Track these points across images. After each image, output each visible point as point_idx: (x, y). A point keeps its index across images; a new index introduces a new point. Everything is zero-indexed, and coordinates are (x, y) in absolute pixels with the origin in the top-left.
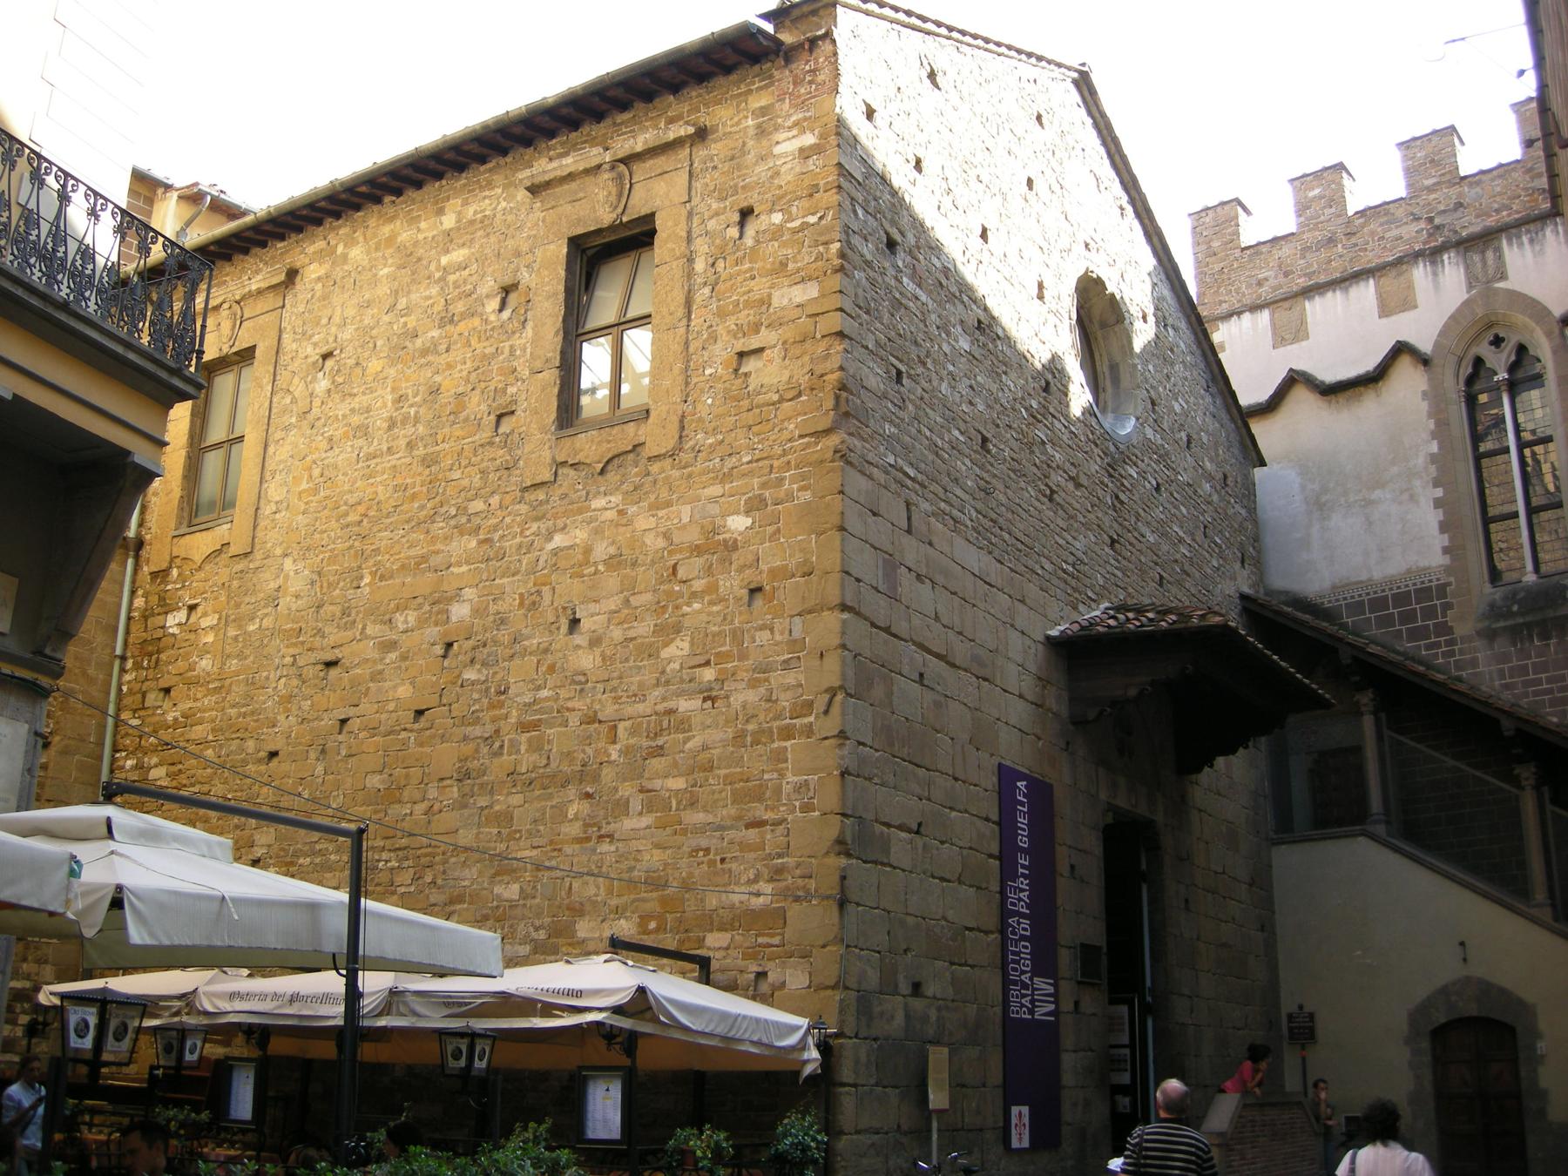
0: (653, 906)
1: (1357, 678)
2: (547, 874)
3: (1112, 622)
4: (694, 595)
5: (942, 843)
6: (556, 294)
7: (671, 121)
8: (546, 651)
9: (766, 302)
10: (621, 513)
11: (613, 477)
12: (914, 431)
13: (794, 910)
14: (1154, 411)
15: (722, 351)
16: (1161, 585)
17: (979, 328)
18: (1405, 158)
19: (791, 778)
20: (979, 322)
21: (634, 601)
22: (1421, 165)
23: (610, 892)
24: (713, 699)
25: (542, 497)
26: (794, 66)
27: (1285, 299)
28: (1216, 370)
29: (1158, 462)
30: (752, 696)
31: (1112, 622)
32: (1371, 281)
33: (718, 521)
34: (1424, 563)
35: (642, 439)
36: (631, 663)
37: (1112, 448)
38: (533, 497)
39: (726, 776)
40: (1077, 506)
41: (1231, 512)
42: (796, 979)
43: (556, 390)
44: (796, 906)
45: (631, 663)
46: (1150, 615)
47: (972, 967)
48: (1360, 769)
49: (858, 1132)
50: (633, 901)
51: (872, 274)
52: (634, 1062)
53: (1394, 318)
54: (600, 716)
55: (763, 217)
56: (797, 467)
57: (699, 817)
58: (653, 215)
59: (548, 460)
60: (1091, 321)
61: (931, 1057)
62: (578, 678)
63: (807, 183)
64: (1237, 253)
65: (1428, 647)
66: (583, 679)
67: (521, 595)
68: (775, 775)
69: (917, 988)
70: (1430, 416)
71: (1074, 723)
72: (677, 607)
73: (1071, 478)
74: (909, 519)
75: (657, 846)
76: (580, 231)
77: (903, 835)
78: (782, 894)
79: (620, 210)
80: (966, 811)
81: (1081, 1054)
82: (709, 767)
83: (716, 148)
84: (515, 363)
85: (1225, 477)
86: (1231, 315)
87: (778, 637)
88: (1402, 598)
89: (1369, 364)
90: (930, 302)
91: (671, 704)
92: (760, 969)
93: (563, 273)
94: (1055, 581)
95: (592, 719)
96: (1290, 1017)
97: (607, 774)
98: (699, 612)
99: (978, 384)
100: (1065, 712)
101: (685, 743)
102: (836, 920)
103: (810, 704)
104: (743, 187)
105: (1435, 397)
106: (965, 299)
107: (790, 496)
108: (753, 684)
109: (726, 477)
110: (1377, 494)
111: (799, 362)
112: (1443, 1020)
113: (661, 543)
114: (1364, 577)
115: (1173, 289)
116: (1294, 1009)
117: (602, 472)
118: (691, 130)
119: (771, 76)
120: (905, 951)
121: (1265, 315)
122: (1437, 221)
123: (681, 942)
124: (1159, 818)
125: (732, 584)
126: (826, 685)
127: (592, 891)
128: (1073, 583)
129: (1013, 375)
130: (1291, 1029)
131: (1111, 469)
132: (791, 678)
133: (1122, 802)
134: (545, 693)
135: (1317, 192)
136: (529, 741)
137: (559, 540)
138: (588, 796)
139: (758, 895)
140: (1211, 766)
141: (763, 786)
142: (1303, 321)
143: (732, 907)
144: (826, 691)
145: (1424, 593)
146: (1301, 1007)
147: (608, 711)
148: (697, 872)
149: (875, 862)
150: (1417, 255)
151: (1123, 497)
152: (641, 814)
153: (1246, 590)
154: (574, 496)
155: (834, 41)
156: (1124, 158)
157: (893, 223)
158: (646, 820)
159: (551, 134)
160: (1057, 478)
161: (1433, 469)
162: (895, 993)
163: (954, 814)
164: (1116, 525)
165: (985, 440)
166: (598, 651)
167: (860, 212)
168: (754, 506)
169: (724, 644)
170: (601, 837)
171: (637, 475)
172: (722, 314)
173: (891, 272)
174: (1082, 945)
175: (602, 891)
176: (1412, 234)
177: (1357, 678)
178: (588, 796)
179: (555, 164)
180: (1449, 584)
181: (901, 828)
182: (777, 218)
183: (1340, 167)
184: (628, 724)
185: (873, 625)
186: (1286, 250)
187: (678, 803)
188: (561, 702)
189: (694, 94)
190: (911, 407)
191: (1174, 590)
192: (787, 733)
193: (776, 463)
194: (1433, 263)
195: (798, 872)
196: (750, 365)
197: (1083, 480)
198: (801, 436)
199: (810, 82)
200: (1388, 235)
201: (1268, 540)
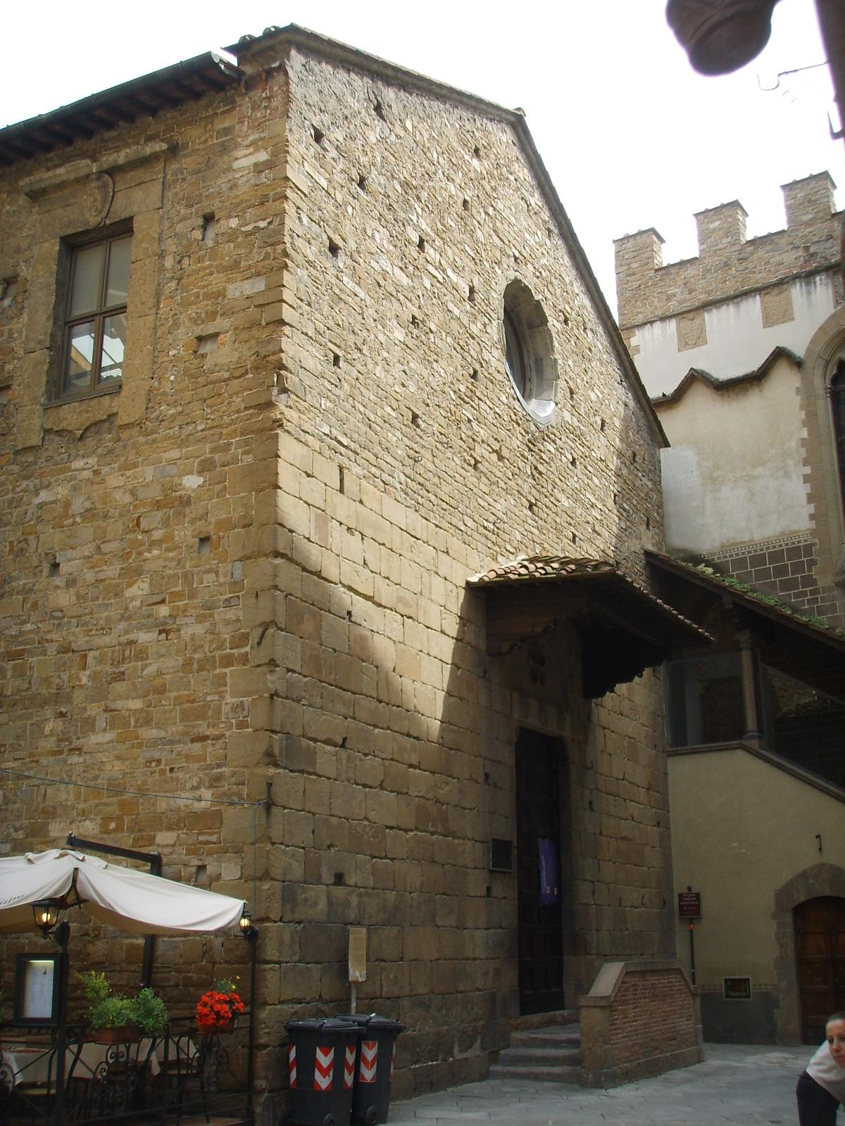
0: (114, 810)
1: (737, 621)
2: (26, 782)
3: (523, 571)
4: (153, 544)
5: (366, 755)
6: (48, 285)
7: (149, 139)
8: (31, 590)
9: (221, 294)
10: (96, 473)
11: (90, 442)
12: (348, 406)
13: (229, 813)
14: (572, 398)
15: (185, 333)
16: (574, 541)
17: (413, 323)
18: (787, 198)
19: (229, 700)
20: (414, 318)
21: (105, 548)
22: (800, 204)
23: (78, 797)
24: (167, 632)
25: (31, 459)
26: (252, 93)
27: (689, 311)
28: (629, 368)
29: (574, 441)
30: (199, 629)
31: (523, 571)
32: (758, 297)
33: (176, 480)
34: (794, 527)
35: (115, 410)
36: (100, 601)
37: (533, 428)
38: (23, 459)
39: (176, 698)
40: (500, 474)
41: (638, 483)
42: (230, 871)
43: (46, 367)
44: (231, 810)
45: (100, 601)
46: (555, 565)
47: (392, 859)
48: (740, 694)
49: (281, 1003)
50: (96, 806)
51: (314, 272)
52: (65, 949)
53: (775, 328)
54: (74, 646)
55: (222, 222)
56: (242, 434)
57: (152, 733)
58: (131, 218)
59: (37, 428)
60: (520, 322)
61: (351, 937)
62: (56, 614)
63: (260, 193)
64: (652, 273)
65: (796, 596)
66: (60, 615)
67: (11, 543)
68: (216, 697)
69: (339, 879)
70: (802, 407)
71: (491, 655)
72: (140, 553)
73: (494, 451)
74: (342, 480)
75: (118, 758)
76: (70, 231)
77: (329, 748)
78: (218, 799)
79: (104, 214)
80: (388, 728)
81: (493, 931)
82: (161, 691)
83: (187, 162)
84: (13, 344)
85: (634, 455)
86: (645, 324)
87: (222, 579)
88: (776, 556)
89: (754, 365)
90: (368, 299)
91: (132, 636)
92: (200, 863)
93: (55, 267)
94: (476, 536)
95: (66, 649)
96: (680, 896)
97: (78, 697)
98: (158, 557)
99: (411, 369)
100: (482, 645)
101: (143, 670)
102: (264, 821)
103: (245, 637)
104: (206, 196)
105: (806, 392)
106: (401, 298)
107: (235, 460)
108: (200, 619)
109: (182, 443)
110: (759, 471)
111: (247, 346)
112: (802, 899)
113: (128, 498)
114: (746, 538)
115: (592, 299)
116: (685, 891)
117: (82, 438)
118: (164, 146)
119: (234, 102)
120: (329, 847)
121: (672, 325)
122: (812, 250)
123: (136, 840)
124: (567, 734)
125: (185, 534)
126: (259, 621)
127: (63, 796)
128: (493, 538)
129: (443, 363)
130: (681, 907)
131: (531, 444)
132: (231, 614)
133: (533, 722)
134: (28, 627)
135: (717, 224)
136: (14, 667)
137: (44, 496)
138: (62, 715)
139: (200, 800)
140: (612, 691)
141: (206, 706)
142: (702, 330)
143: (178, 810)
144: (260, 625)
145: (794, 552)
146: (689, 889)
147: (80, 642)
148: (150, 780)
149: (302, 772)
150: (796, 277)
151: (541, 468)
152: (105, 730)
153: (650, 548)
154: (58, 459)
155: (286, 73)
156: (553, 189)
157: (336, 230)
158: (109, 736)
159: (48, 148)
160: (480, 451)
161: (803, 451)
162: (319, 882)
163: (377, 730)
164: (534, 491)
165: (415, 417)
166: (73, 591)
167: (305, 219)
168: (205, 467)
169: (176, 586)
170: (71, 750)
171: (110, 441)
172: (186, 304)
173: (332, 271)
174: (493, 840)
175: (71, 797)
176: (791, 260)
177: (737, 621)
178: (62, 715)
179: (50, 174)
180: (814, 544)
181: (327, 742)
182: (234, 223)
183: (735, 205)
184: (96, 653)
185: (304, 569)
186: (691, 271)
187: (136, 721)
188: (41, 634)
189: (169, 115)
190: (346, 387)
191: (585, 545)
192: (228, 661)
193: (225, 431)
194: (808, 284)
195: (234, 779)
196: (207, 348)
197: (505, 453)
198: (246, 408)
199: (266, 108)
200: (772, 260)
201: (670, 508)
